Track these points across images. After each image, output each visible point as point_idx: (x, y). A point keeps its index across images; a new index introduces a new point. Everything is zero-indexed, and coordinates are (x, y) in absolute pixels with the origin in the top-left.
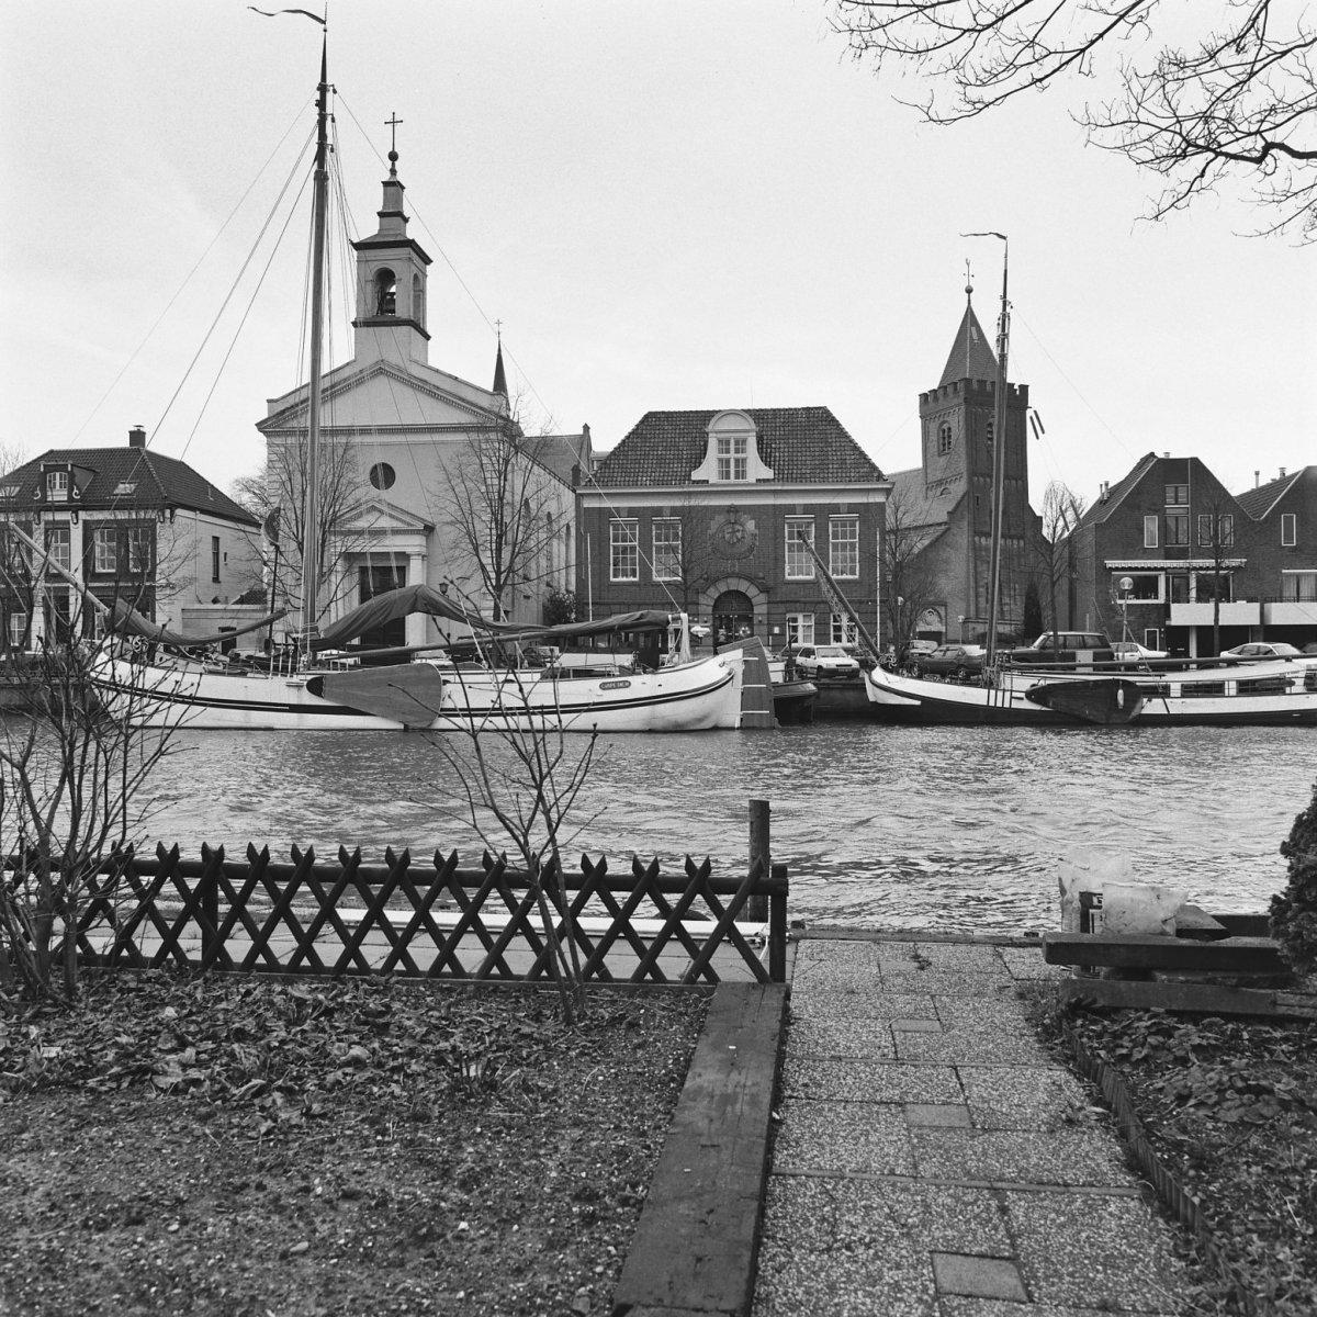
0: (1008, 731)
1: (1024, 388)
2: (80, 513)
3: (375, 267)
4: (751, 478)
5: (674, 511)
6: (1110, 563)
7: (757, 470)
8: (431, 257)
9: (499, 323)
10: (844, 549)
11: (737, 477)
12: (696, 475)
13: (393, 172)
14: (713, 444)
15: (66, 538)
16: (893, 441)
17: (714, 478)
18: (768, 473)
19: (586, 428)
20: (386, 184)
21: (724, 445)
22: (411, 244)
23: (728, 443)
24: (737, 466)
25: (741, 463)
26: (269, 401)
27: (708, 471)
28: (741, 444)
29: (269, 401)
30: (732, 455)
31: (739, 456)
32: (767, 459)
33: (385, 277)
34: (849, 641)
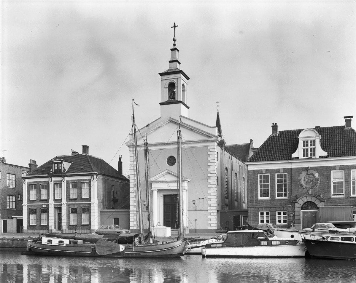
2: (26, 179)
3: (168, 82)
4: (317, 156)
5: (285, 170)
6: (13, 217)
7: (320, 152)
8: (190, 78)
9: (218, 102)
10: (282, 186)
11: (311, 155)
12: (294, 155)
13: (175, 45)
14: (301, 143)
15: (61, 187)
17: (301, 156)
18: (325, 154)
19: (251, 140)
20: (172, 50)
21: (305, 143)
22: (181, 72)
23: (307, 142)
25: (313, 151)
27: (299, 153)
28: (313, 143)
30: (309, 147)
31: (306, 147)
32: (324, 148)
33: (172, 86)
34: (284, 222)
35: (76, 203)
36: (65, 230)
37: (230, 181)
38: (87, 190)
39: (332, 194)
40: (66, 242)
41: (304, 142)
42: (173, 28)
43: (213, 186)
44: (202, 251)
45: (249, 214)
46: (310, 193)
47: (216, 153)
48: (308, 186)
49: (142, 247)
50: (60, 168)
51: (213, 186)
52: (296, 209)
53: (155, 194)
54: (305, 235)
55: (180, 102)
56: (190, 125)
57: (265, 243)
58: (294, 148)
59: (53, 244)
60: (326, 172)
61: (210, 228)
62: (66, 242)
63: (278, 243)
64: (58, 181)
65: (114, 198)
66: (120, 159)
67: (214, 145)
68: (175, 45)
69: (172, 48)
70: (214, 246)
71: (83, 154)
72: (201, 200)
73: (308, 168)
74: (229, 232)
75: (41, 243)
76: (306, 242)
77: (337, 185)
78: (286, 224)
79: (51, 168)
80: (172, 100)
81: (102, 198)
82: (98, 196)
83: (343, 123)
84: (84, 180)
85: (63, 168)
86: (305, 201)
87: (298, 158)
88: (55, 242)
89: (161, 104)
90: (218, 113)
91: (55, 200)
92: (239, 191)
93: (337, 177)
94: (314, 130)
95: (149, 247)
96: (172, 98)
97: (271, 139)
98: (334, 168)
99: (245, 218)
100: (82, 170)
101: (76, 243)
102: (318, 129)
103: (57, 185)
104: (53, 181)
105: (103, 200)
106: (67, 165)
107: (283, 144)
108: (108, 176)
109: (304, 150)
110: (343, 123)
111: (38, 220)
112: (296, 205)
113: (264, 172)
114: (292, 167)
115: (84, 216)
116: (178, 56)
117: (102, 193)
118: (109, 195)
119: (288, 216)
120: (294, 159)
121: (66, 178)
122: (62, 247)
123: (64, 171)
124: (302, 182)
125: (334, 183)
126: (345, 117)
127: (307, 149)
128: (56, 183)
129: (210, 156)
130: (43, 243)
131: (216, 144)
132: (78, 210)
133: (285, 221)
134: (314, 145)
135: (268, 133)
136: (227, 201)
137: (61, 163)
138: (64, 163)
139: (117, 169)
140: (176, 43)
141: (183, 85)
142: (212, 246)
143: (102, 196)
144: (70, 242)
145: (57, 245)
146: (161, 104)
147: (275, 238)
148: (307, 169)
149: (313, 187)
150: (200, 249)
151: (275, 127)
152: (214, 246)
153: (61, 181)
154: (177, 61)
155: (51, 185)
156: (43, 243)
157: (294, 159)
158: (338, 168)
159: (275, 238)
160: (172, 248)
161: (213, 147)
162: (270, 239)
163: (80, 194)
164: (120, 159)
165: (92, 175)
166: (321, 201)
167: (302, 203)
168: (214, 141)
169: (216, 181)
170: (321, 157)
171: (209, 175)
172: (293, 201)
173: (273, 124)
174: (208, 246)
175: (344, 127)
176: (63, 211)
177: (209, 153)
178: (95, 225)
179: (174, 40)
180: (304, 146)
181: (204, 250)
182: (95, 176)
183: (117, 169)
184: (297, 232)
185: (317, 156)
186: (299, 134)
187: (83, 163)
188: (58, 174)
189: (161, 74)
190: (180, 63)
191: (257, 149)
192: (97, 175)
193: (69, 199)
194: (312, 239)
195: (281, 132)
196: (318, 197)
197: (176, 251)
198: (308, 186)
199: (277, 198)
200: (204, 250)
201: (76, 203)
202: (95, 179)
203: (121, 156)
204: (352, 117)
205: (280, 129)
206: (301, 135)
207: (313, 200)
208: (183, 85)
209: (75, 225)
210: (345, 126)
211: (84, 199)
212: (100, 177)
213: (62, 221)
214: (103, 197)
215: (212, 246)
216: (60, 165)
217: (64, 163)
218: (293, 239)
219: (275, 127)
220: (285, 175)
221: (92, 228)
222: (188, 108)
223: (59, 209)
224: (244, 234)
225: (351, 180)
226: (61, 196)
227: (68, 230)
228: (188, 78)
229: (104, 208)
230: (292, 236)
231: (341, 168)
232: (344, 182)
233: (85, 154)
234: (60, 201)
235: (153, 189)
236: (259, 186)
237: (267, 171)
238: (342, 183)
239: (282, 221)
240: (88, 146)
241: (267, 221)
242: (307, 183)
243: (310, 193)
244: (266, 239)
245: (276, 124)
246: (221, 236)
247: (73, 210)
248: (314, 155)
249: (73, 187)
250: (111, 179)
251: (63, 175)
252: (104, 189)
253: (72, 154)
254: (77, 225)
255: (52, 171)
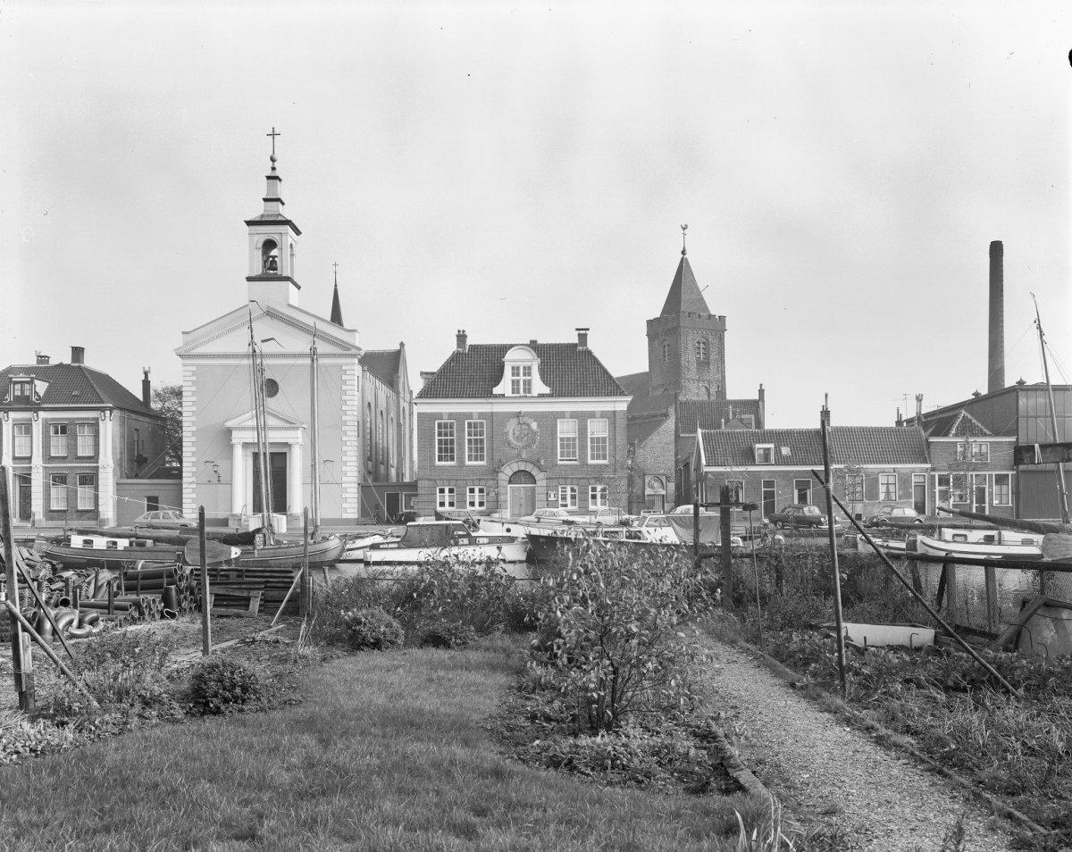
0: (970, 567)
1: (722, 318)
3: (262, 239)
4: (535, 392)
5: (481, 415)
7: (539, 387)
11: (525, 392)
12: (496, 390)
13: (274, 169)
16: (626, 355)
17: (509, 393)
18: (547, 390)
19: (402, 345)
21: (515, 371)
22: (287, 222)
23: (518, 368)
24: (524, 384)
25: (528, 384)
26: (183, 333)
27: (504, 387)
28: (528, 371)
29: (183, 333)
30: (522, 378)
35: (65, 465)
36: (40, 520)
37: (373, 427)
38: (90, 441)
39: (559, 458)
40: (123, 543)
41: (513, 368)
42: (271, 137)
43: (351, 438)
44: (365, 555)
45: (420, 491)
46: (524, 456)
47: (356, 378)
48: (520, 444)
49: (272, 551)
50: (27, 393)
51: (351, 438)
52: (501, 483)
53: (238, 452)
54: (530, 529)
55: (288, 279)
56: (335, 335)
57: (466, 541)
58: (497, 377)
59: (95, 547)
60: (549, 420)
61: (345, 516)
62: (123, 543)
63: (486, 540)
64: (25, 420)
65: (139, 455)
66: (146, 374)
67: (353, 364)
68: (274, 169)
69: (268, 174)
70: (386, 546)
71: (73, 365)
72: (328, 464)
73: (520, 413)
74: (409, 524)
75: (68, 546)
76: (532, 538)
77: (567, 443)
78: (483, 508)
79: (7, 391)
80: (270, 271)
81: (118, 457)
82: (113, 453)
83: (576, 340)
84: (83, 419)
85: (35, 392)
86: (516, 469)
87: (503, 396)
88: (100, 543)
89: (249, 279)
90: (336, 285)
91: (15, 458)
92: (385, 445)
93: (566, 429)
94: (529, 348)
95: (285, 550)
96: (269, 269)
97: (455, 358)
98: (562, 415)
99: (409, 497)
100: (76, 399)
101: (142, 545)
102: (533, 345)
103: (21, 429)
104: (11, 421)
105: (121, 459)
106: (41, 387)
107: (474, 368)
108: (129, 411)
109: (513, 381)
110: (576, 340)
111: (71, 497)
112: (501, 476)
113: (445, 417)
114: (494, 410)
115: (84, 492)
116: (282, 190)
117: (118, 446)
118: (130, 450)
119: (488, 494)
120: (496, 396)
121: (42, 414)
122: (116, 553)
123: (37, 400)
124: (511, 437)
125: (562, 439)
126: (577, 329)
127: (518, 381)
128: (16, 424)
129: (345, 382)
130: (72, 546)
131: (356, 361)
132: (69, 480)
133: (481, 504)
134: (530, 375)
135: (452, 347)
136: (370, 464)
137: (31, 382)
138: (36, 382)
139: (141, 398)
140: (276, 164)
141: (291, 245)
142: (381, 546)
143: (118, 451)
144: (131, 544)
145: (81, 547)
146: (249, 279)
147: (480, 533)
148: (518, 415)
149: (529, 446)
150: (361, 552)
151: (461, 337)
152: (386, 546)
153: (30, 420)
154: (278, 200)
155: (37, 429)
156: (72, 546)
157: (496, 396)
158: (568, 415)
159: (480, 533)
160: (324, 552)
161: (350, 367)
162: (473, 534)
163: (72, 447)
164: (146, 374)
165: (103, 410)
166: (541, 469)
167: (510, 473)
168: (353, 356)
169: (356, 429)
170: (541, 396)
171: (344, 418)
172: (495, 471)
173: (459, 331)
174: (375, 547)
175: (575, 345)
176: (33, 483)
177: (344, 377)
178: (108, 511)
179: (273, 160)
180: (513, 375)
181: (369, 554)
182: (108, 413)
183: (141, 398)
184: (516, 523)
185: (535, 392)
186: (506, 352)
187: (75, 384)
188: (24, 406)
189: (249, 223)
190: (283, 204)
191: (432, 374)
192: (111, 410)
193: (48, 458)
194: (542, 534)
195: (473, 347)
196: (536, 463)
197: (332, 556)
198: (520, 444)
199: (467, 463)
200: (369, 554)
201: (65, 465)
202: (108, 419)
203: (147, 369)
204: (588, 329)
205: (470, 341)
206: (510, 356)
207: (529, 468)
208: (291, 245)
209: (61, 511)
210: (576, 344)
211: (55, 457)
212: (116, 413)
213: (33, 503)
214: (121, 453)
215: (381, 546)
216: (27, 386)
217: (36, 382)
218: (508, 534)
219: (461, 337)
220: (482, 424)
221: (102, 517)
222: (299, 288)
223: (25, 479)
224: (434, 528)
225: (589, 435)
226: (29, 451)
227: (47, 520)
228: (298, 232)
229: (121, 477)
230: (508, 530)
231: (574, 415)
232: (577, 440)
233: (76, 365)
234: (27, 461)
235: (234, 441)
236: (437, 441)
237: (451, 415)
238: (574, 439)
239: (477, 504)
240: (83, 349)
241: (451, 504)
242: (518, 439)
243: (524, 456)
244: (468, 535)
245: (463, 331)
246: (389, 531)
247: (60, 479)
248: (530, 392)
249: (56, 433)
250: (134, 416)
251: (36, 409)
252: (122, 437)
253: (38, 362)
254: (65, 511)
255: (9, 398)
